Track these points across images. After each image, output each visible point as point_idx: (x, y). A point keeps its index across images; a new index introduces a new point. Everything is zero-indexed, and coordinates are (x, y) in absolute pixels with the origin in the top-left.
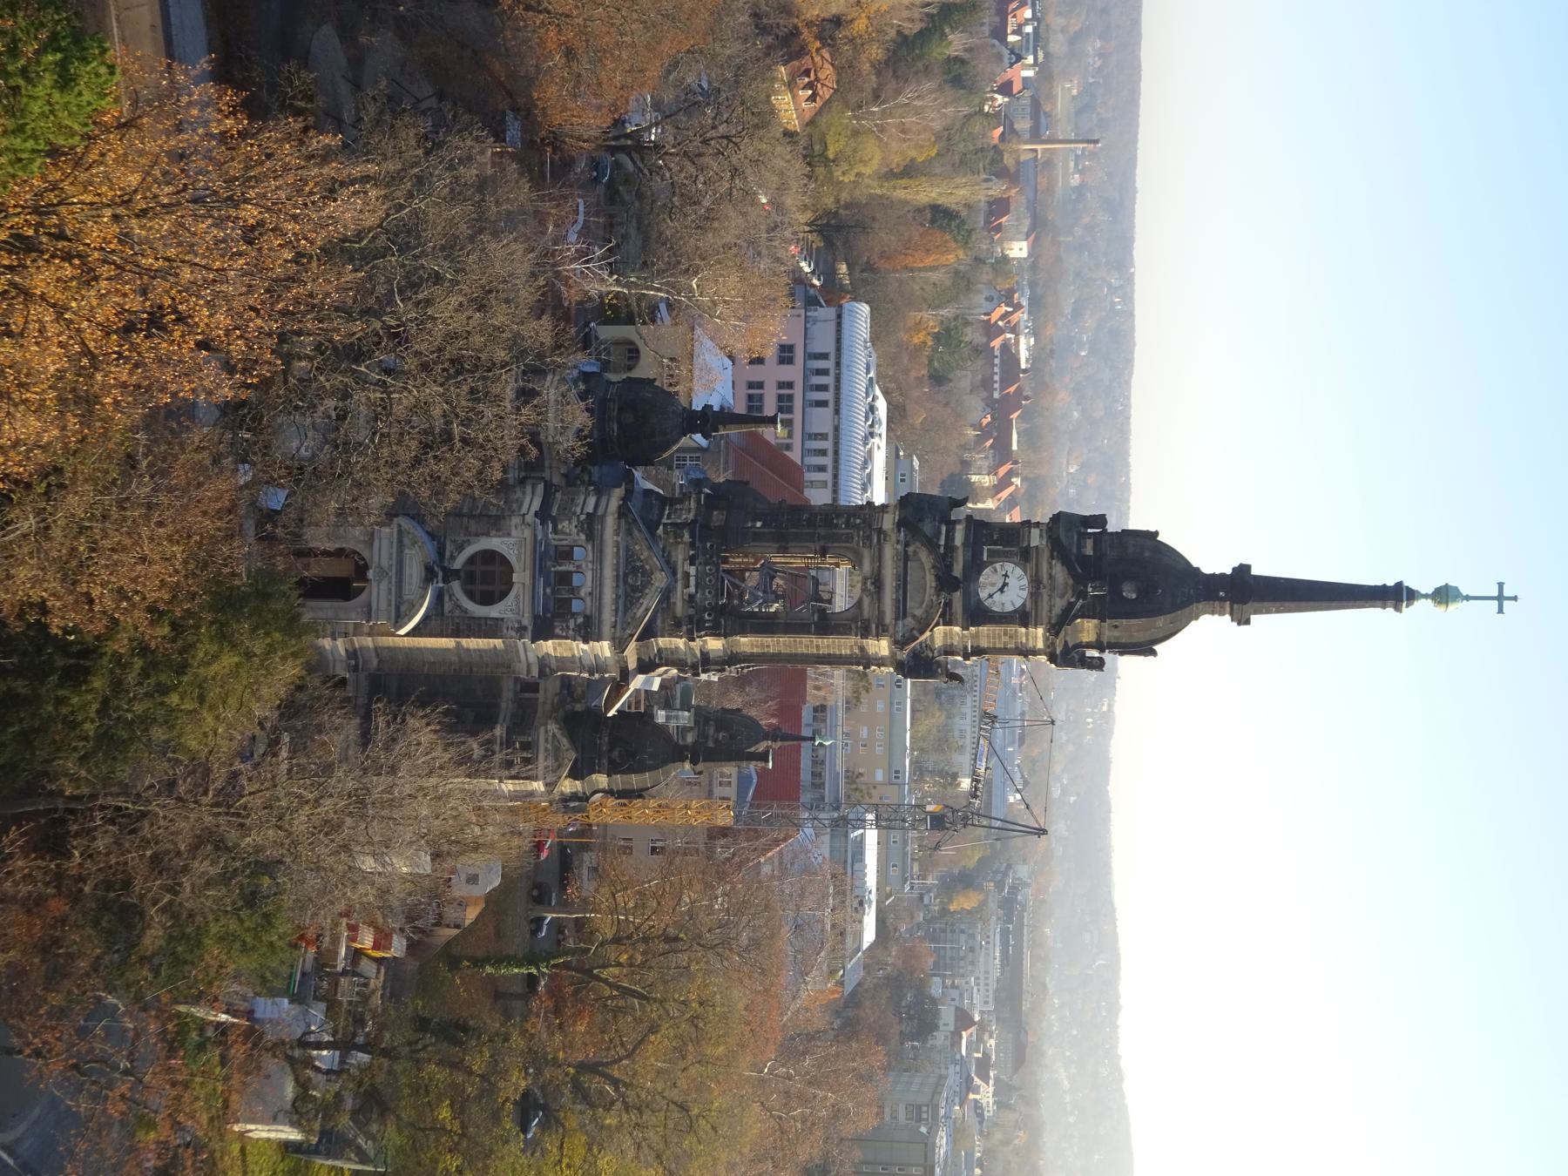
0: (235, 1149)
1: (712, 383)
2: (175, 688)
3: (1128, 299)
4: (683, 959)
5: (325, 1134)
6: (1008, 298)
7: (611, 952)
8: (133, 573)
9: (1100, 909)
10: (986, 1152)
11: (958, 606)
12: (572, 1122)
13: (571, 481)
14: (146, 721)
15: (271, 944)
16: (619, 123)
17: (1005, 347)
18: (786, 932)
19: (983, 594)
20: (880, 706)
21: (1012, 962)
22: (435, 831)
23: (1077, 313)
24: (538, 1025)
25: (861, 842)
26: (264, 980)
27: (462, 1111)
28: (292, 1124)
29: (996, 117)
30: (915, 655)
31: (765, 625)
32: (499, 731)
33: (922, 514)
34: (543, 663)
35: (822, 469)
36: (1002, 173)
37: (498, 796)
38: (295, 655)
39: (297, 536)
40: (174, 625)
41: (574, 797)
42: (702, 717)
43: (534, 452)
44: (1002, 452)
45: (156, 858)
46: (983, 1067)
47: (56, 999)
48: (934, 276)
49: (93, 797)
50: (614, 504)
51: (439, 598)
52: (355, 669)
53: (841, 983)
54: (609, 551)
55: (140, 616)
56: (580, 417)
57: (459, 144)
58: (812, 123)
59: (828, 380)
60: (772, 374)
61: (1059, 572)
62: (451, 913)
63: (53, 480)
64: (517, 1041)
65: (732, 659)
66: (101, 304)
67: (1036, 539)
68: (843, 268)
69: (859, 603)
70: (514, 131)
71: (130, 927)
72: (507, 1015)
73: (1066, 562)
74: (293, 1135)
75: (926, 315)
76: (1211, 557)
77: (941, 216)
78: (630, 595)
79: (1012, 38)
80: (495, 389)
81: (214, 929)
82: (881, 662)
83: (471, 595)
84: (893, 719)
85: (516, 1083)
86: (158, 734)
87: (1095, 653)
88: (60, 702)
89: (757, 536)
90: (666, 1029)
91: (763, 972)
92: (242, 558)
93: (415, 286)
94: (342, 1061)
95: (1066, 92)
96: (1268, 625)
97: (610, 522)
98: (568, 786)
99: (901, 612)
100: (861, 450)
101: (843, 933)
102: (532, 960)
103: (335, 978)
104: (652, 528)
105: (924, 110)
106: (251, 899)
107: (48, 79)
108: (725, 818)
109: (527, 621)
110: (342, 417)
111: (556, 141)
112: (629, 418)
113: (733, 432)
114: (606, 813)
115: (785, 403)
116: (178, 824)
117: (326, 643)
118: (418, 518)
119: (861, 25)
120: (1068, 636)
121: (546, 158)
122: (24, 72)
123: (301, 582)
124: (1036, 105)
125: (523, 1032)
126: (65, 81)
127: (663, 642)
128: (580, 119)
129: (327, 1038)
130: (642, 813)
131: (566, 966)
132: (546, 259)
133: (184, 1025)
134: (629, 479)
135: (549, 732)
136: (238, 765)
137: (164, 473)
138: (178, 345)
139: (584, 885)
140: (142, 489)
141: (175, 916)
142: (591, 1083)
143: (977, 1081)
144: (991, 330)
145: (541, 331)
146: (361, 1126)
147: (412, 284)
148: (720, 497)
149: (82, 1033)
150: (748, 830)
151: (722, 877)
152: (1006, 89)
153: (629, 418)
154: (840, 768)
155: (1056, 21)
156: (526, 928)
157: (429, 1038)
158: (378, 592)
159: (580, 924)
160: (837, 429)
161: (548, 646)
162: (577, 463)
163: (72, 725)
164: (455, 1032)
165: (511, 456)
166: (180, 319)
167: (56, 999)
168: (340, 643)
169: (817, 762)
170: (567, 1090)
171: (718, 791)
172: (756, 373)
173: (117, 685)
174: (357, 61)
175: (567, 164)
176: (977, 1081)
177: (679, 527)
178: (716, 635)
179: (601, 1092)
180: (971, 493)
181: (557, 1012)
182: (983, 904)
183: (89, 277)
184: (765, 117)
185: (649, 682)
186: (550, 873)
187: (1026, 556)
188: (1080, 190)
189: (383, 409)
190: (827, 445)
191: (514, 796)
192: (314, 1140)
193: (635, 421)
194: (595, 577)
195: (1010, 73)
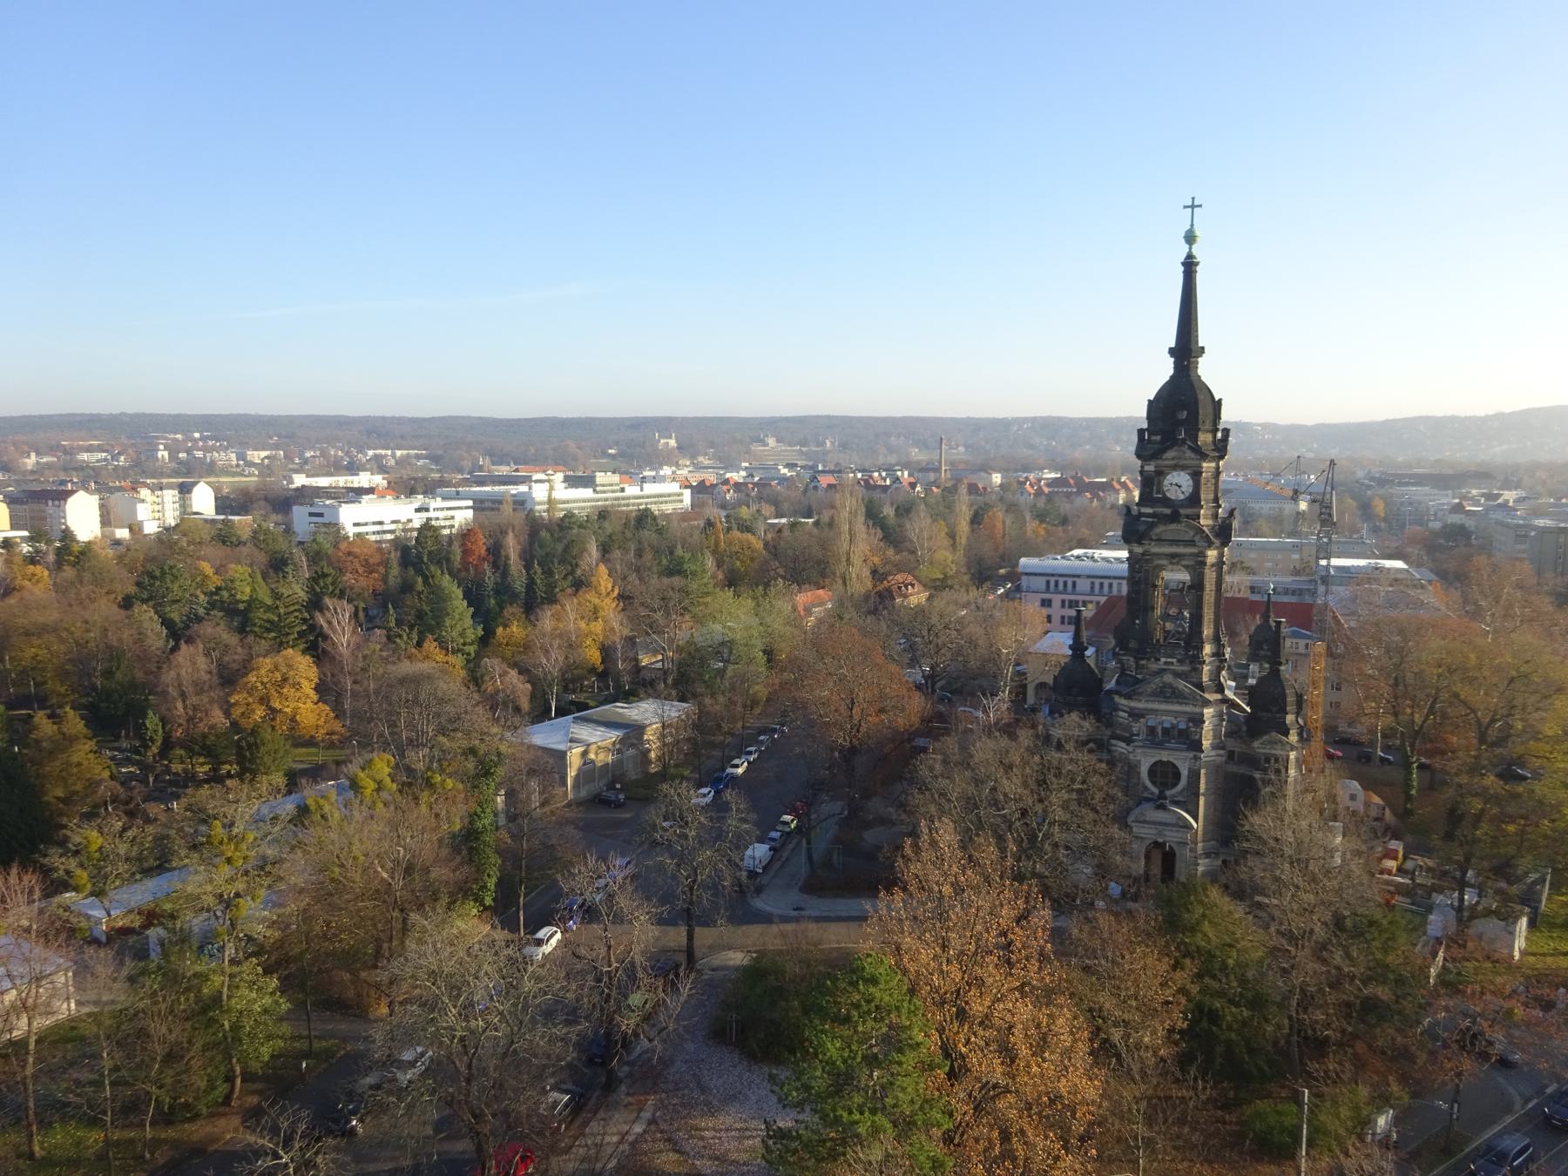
0: (1531, 959)
1: (1059, 643)
2: (1223, 962)
3: (1025, 420)
10: (1551, 496)
11: (1189, 511)
12: (1520, 750)
13: (1110, 724)
14: (1243, 981)
15: (1391, 923)
16: (918, 687)
17: (1048, 485)
18: (1394, 614)
19: (1182, 497)
20: (1252, 555)
21: (1420, 480)
22: (1315, 815)
23: (1031, 447)
25: (1338, 568)
26: (1415, 929)
27: (1511, 817)
28: (1515, 923)
29: (927, 490)
30: (1217, 535)
31: (1197, 620)
32: (1257, 775)
33: (1134, 530)
35: (1111, 585)
38: (1205, 889)
39: (1136, 880)
40: (1184, 956)
41: (1300, 734)
43: (1091, 745)
44: (1106, 487)
46: (1490, 497)
47: (1422, 1057)
48: (1008, 522)
49: (1290, 1018)
50: (1123, 701)
51: (1177, 803)
52: (1217, 854)
53: (1430, 582)
55: (1178, 975)
57: (924, 772)
59: (1061, 580)
60: (1057, 611)
61: (1170, 454)
62: (1374, 813)
64: (1464, 779)
65: (1216, 639)
66: (991, 972)
67: (1150, 468)
68: (1002, 571)
69: (1186, 567)
70: (921, 742)
72: (1445, 783)
73: (1164, 451)
74: (1524, 922)
76: (1164, 369)
77: (976, 520)
78: (1174, 695)
80: (1055, 763)
81: (1379, 956)
82: (1221, 555)
83: (1175, 785)
84: (1263, 548)
86: (1250, 974)
87: (1219, 435)
88: (1230, 1028)
89: (1145, 622)
90: (1457, 688)
91: (1419, 629)
94: (1472, 886)
95: (916, 454)
96: (1205, 334)
97: (1133, 704)
98: (1293, 738)
99: (1191, 543)
100: (1101, 564)
101: (1395, 579)
102: (1408, 766)
104: (1138, 681)
105: (920, 527)
108: (1320, 647)
109: (1191, 755)
110: (1067, 848)
113: (1085, 634)
114: (1316, 716)
116: (1308, 971)
117: (1200, 869)
118: (1128, 811)
119: (876, 560)
121: (935, 725)
122: (868, 1002)
123: (1163, 880)
124: (922, 470)
125: (1456, 775)
126: (873, 981)
127: (1205, 679)
128: (917, 705)
129: (1456, 894)
130: (1317, 695)
131: (1412, 745)
132: (988, 730)
133: (1443, 980)
134: (1110, 692)
136: (1272, 929)
137: (1094, 951)
138: (1018, 936)
139: (1360, 731)
141: (1370, 979)
142: (1494, 735)
143: (1500, 501)
144: (1039, 492)
145: (1025, 736)
147: (995, 804)
148: (1122, 643)
151: (1357, 649)
152: (913, 485)
154: (1290, 579)
155: (881, 460)
157: (1458, 833)
158: (1171, 837)
159: (1384, 736)
160: (1088, 577)
161: (1206, 744)
162: (1098, 720)
163: (1244, 1023)
164: (1454, 817)
169: (1286, 592)
170: (1498, 751)
171: (1302, 650)
172: (1056, 619)
173: (1220, 994)
176: (1500, 501)
177: (1138, 666)
178: (1202, 648)
179: (1500, 729)
181: (1443, 753)
182: (1381, 497)
183: (980, 982)
184: (920, 611)
185: (1230, 688)
186: (1348, 750)
187: (1160, 473)
188: (966, 446)
189: (1063, 824)
190: (1097, 582)
192: (1527, 910)
193: (1077, 687)
194: (1167, 714)
195: (905, 483)
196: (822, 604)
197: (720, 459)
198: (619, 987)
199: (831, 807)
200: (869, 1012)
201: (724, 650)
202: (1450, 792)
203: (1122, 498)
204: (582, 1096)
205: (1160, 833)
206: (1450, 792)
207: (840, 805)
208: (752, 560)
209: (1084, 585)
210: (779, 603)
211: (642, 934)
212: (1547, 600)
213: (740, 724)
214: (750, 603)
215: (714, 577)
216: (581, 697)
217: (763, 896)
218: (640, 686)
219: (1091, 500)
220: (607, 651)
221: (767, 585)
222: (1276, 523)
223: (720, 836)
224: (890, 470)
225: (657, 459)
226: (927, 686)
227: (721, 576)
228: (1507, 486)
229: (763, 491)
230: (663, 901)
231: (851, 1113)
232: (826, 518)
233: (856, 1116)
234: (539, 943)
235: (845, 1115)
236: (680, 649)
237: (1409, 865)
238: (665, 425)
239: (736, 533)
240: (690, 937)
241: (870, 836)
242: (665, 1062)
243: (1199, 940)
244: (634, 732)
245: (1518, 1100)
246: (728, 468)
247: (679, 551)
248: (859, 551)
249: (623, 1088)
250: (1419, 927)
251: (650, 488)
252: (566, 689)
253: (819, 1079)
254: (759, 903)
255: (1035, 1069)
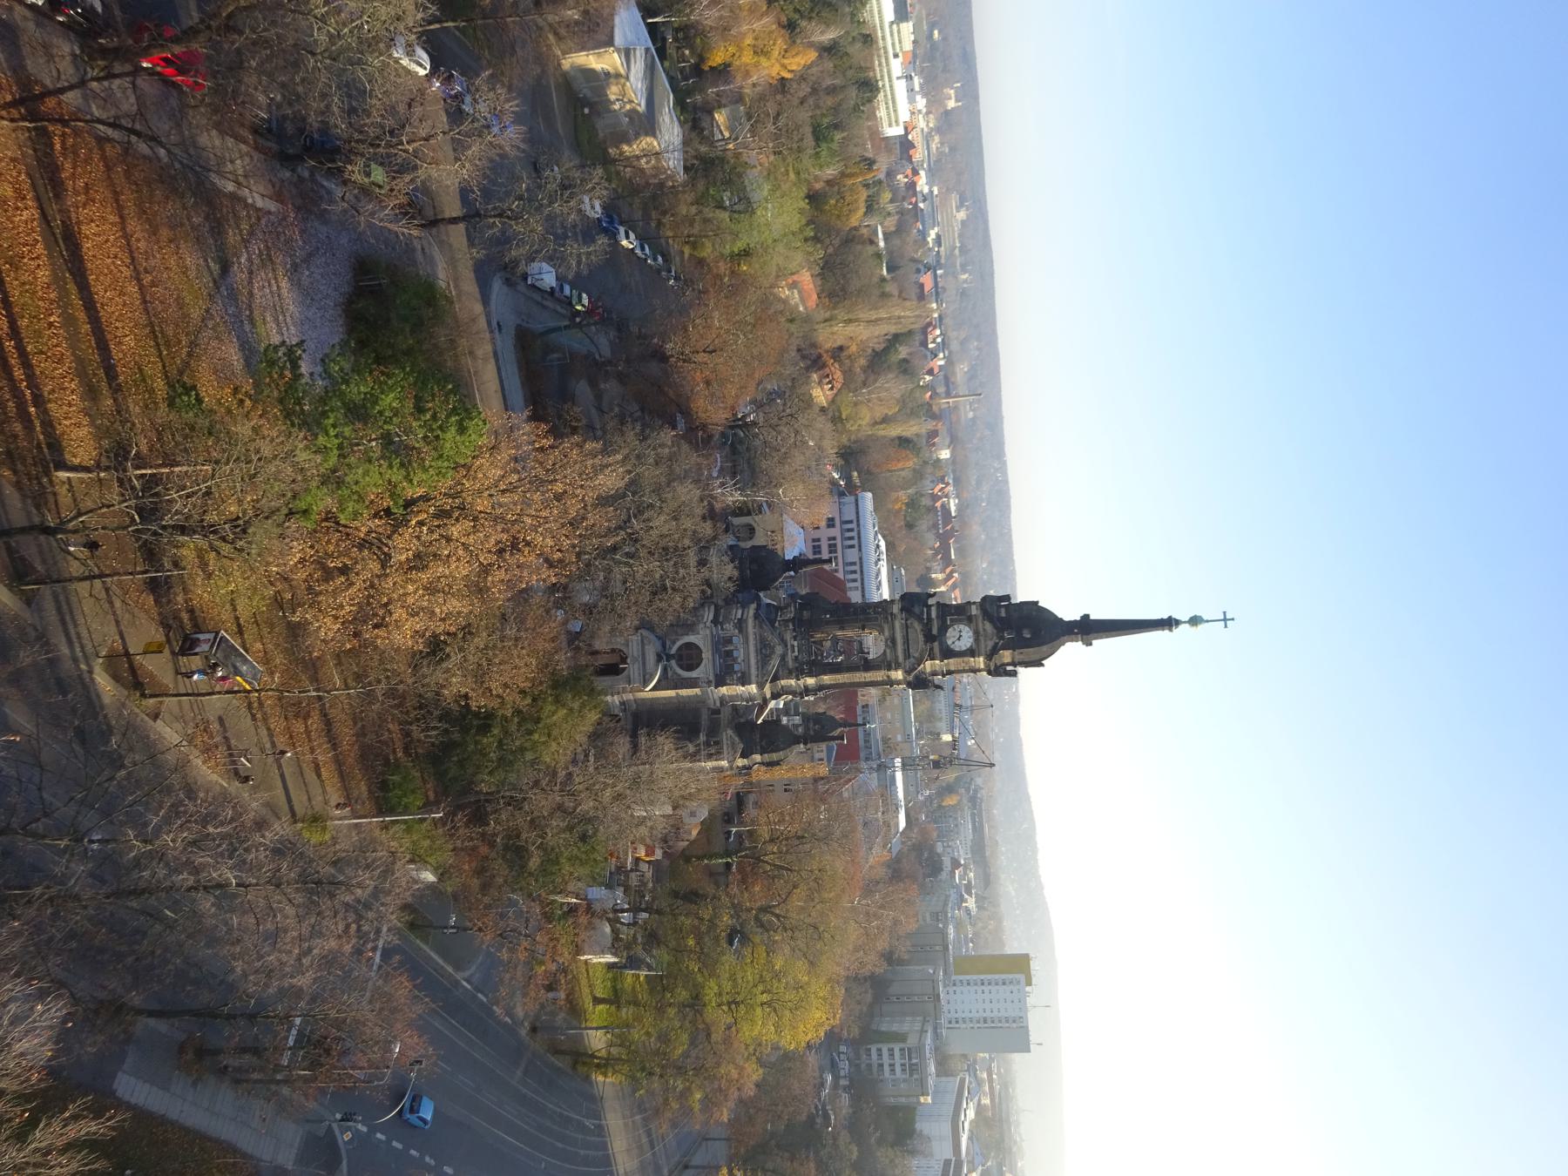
1: (794, 544)
3: (1005, 474)
4: (807, 847)
5: (629, 958)
6: (942, 480)
7: (770, 848)
8: (511, 675)
9: (1022, 797)
12: (757, 939)
13: (728, 602)
14: (522, 750)
16: (735, 415)
18: (860, 828)
21: (978, 830)
22: (676, 791)
23: (979, 483)
24: (734, 890)
26: (594, 879)
29: (927, 387)
30: (916, 677)
31: (835, 669)
32: (702, 738)
33: (913, 603)
34: (722, 699)
36: (934, 417)
37: (702, 771)
41: (744, 767)
42: (806, 718)
44: (946, 557)
45: (532, 821)
46: (968, 888)
47: (486, 900)
50: (752, 612)
51: (665, 670)
54: (751, 637)
56: (730, 570)
58: (833, 401)
59: (854, 534)
60: (825, 533)
61: (988, 626)
63: (468, 631)
65: (821, 688)
67: (974, 611)
70: (681, 424)
71: (521, 858)
73: (991, 621)
74: (610, 959)
75: (901, 493)
77: (904, 442)
78: (764, 660)
79: (931, 346)
85: (726, 920)
86: (529, 756)
87: (1009, 668)
89: (828, 623)
92: (563, 662)
93: (641, 512)
95: (962, 369)
96: (1102, 645)
97: (750, 622)
98: (740, 762)
99: (907, 655)
101: (889, 825)
103: (627, 873)
104: (772, 623)
105: (891, 387)
106: (584, 838)
107: (453, 430)
108: (823, 770)
111: (704, 427)
112: (755, 567)
114: (761, 775)
115: (832, 548)
116: (541, 803)
118: (651, 629)
119: (854, 348)
120: (996, 660)
121: (697, 435)
122: (440, 428)
124: (946, 378)
126: (462, 430)
127: (783, 682)
128: (714, 414)
130: (780, 773)
131: (746, 856)
134: (758, 599)
135: (728, 735)
139: (751, 812)
140: (511, 632)
141: (545, 850)
142: (766, 919)
144: (935, 498)
145: (707, 529)
146: (648, 952)
148: (809, 602)
149: (502, 916)
150: (836, 775)
152: (930, 372)
153: (755, 567)
155: (952, 334)
156: (722, 837)
157: (680, 902)
158: (633, 669)
161: (724, 690)
165: (697, 595)
166: (528, 544)
167: (486, 900)
168: (616, 699)
171: (817, 756)
172: (816, 534)
174: (599, 396)
175: (710, 437)
178: (811, 676)
179: (770, 922)
180: (933, 583)
181: (744, 881)
182: (959, 802)
184: (808, 402)
187: (970, 620)
188: (974, 419)
190: (857, 568)
191: (714, 769)
193: (759, 568)
194: (746, 652)
195: (932, 364)
196: (803, 300)
197: (938, 161)
198: (389, 156)
199: (603, 343)
200: (432, 430)
201: (745, 206)
202: (710, 889)
203: (938, 576)
204: (269, 130)
205: (635, 660)
206: (710, 889)
207: (607, 361)
208: (839, 216)
209: (852, 555)
210: (799, 257)
211: (448, 175)
212: (886, 945)
213: (670, 234)
214: (795, 227)
215: (817, 179)
216: (671, 51)
217: (505, 289)
218: (694, 118)
219: (932, 548)
220: (723, 72)
221: (816, 239)
222: (927, 718)
223: (561, 239)
224: (944, 345)
225: (932, 90)
226: (738, 423)
227: (818, 186)
228: (980, 900)
229: (909, 218)
230: (487, 194)
231: (334, 426)
232: (891, 288)
233: (332, 432)
234: (410, 53)
235: (331, 421)
236: (737, 156)
237: (644, 867)
238: (970, 94)
239: (864, 194)
240: (454, 221)
241: (582, 388)
242: (323, 216)
243: (549, 708)
244: (646, 123)
245: (467, 974)
246: (931, 173)
247: (838, 136)
248: (858, 331)
249: (288, 174)
250: (594, 880)
251: (900, 87)
252: (677, 30)
253: (357, 390)
254: (497, 286)
255: (411, 588)
